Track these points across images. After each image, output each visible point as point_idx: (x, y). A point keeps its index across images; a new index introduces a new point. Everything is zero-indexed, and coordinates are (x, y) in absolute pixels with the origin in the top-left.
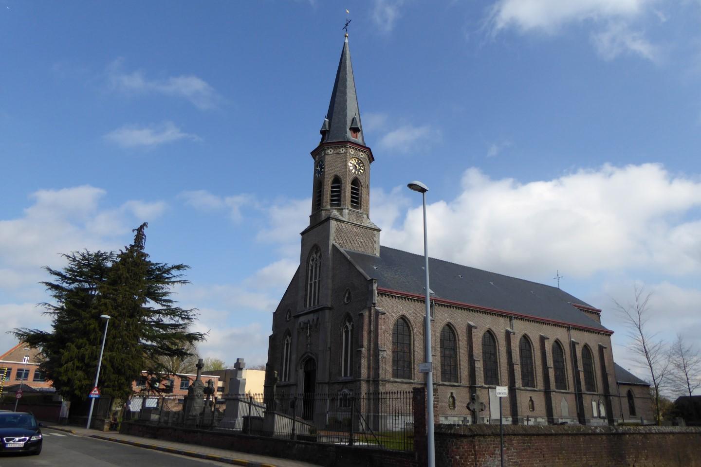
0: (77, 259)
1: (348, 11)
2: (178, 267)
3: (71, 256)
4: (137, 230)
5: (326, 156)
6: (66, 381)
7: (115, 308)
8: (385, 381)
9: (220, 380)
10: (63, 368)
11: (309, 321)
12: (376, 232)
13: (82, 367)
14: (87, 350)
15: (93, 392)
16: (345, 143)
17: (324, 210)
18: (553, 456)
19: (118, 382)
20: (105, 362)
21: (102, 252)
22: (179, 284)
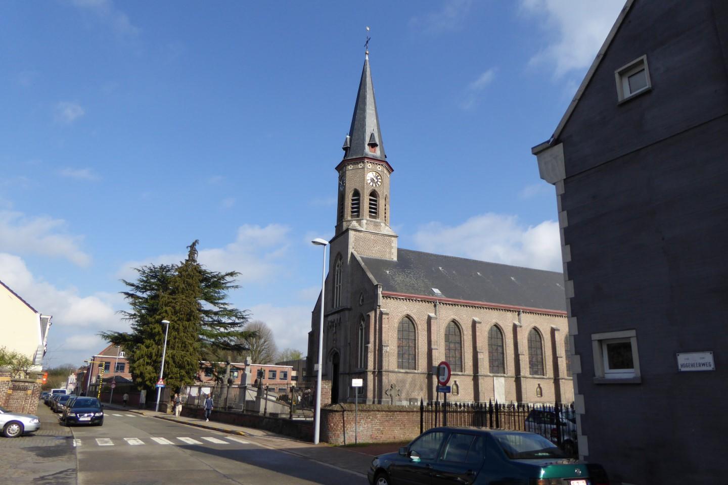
0: (147, 272)
1: (368, 29)
2: (232, 274)
3: (141, 270)
4: (191, 247)
5: (347, 172)
6: (139, 374)
7: (175, 313)
8: (388, 371)
9: (293, 369)
10: (136, 363)
11: (334, 320)
13: (151, 363)
14: (153, 349)
15: (159, 383)
16: (361, 160)
17: (345, 221)
18: (414, 426)
19: (180, 374)
20: (168, 359)
21: (165, 265)
22: (233, 289)
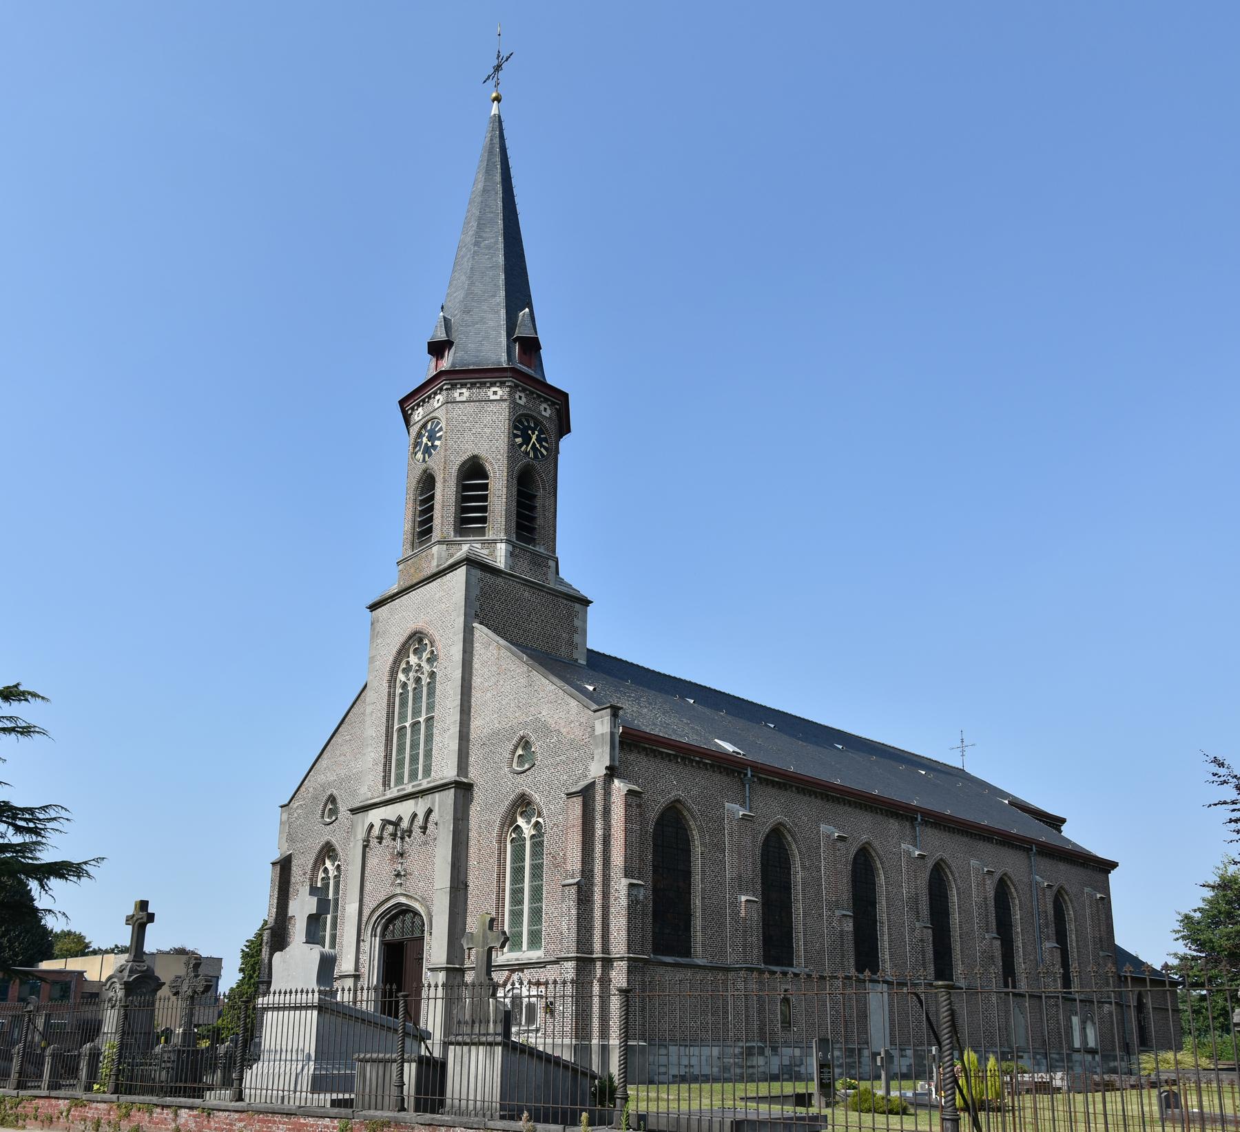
12: (577, 606)
